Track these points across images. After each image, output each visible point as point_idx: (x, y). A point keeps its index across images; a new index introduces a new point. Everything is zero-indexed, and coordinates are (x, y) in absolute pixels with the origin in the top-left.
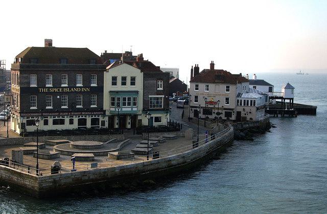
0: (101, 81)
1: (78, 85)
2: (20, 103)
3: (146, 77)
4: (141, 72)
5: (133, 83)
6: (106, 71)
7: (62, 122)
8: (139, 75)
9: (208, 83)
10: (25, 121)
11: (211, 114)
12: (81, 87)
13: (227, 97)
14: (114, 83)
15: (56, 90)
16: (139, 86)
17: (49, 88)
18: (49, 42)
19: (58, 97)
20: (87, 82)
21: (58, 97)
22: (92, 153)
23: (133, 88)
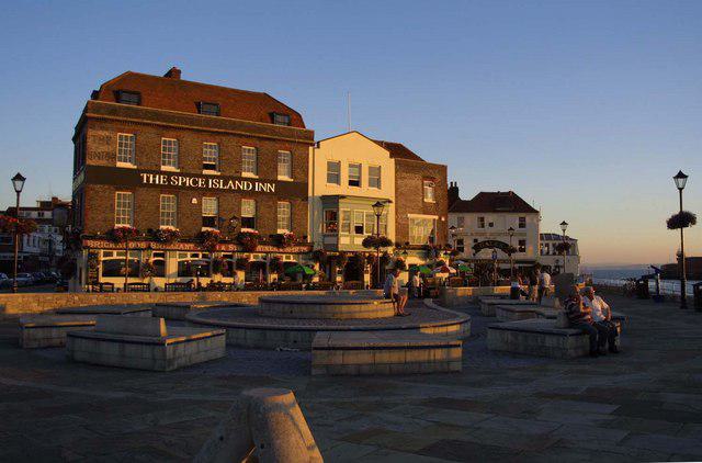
0: (300, 167)
1: (244, 175)
2: (308, 158)
3: (399, 167)
4: (391, 157)
5: (376, 182)
6: (313, 145)
7: (111, 254)
8: (388, 165)
9: (461, 212)
10: (562, 271)
11: (251, 250)
12: (253, 181)
13: (521, 238)
14: (334, 177)
15: (189, 182)
16: (387, 190)
17: (169, 174)
18: (173, 73)
19: (194, 201)
20: (266, 170)
21: (194, 201)
22: (594, 396)
23: (374, 193)
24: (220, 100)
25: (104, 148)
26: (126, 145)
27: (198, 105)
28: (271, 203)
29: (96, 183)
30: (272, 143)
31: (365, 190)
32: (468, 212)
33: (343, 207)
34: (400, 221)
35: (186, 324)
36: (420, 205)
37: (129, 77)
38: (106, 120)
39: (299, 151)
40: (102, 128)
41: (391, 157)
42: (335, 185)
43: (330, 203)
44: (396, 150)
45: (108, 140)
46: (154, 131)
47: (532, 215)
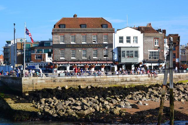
16: (140, 43)
19: (80, 51)
24: (86, 23)
25: (57, 40)
26: (62, 38)
27: (80, 25)
28: (101, 50)
29: (55, 48)
30: (101, 34)
31: (132, 44)
32: (29, 112)
33: (122, 49)
34: (145, 52)
35: (80, 82)
36: (153, 47)
37: (64, 19)
38: (56, 33)
39: (109, 35)
40: (56, 35)
41: (141, 33)
42: (122, 43)
43: (119, 48)
44: (139, 29)
45: (58, 38)
46: (69, 34)
47: (11, 51)
